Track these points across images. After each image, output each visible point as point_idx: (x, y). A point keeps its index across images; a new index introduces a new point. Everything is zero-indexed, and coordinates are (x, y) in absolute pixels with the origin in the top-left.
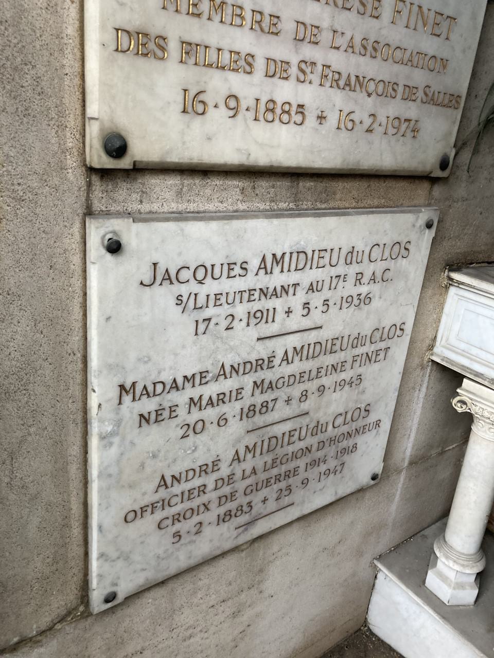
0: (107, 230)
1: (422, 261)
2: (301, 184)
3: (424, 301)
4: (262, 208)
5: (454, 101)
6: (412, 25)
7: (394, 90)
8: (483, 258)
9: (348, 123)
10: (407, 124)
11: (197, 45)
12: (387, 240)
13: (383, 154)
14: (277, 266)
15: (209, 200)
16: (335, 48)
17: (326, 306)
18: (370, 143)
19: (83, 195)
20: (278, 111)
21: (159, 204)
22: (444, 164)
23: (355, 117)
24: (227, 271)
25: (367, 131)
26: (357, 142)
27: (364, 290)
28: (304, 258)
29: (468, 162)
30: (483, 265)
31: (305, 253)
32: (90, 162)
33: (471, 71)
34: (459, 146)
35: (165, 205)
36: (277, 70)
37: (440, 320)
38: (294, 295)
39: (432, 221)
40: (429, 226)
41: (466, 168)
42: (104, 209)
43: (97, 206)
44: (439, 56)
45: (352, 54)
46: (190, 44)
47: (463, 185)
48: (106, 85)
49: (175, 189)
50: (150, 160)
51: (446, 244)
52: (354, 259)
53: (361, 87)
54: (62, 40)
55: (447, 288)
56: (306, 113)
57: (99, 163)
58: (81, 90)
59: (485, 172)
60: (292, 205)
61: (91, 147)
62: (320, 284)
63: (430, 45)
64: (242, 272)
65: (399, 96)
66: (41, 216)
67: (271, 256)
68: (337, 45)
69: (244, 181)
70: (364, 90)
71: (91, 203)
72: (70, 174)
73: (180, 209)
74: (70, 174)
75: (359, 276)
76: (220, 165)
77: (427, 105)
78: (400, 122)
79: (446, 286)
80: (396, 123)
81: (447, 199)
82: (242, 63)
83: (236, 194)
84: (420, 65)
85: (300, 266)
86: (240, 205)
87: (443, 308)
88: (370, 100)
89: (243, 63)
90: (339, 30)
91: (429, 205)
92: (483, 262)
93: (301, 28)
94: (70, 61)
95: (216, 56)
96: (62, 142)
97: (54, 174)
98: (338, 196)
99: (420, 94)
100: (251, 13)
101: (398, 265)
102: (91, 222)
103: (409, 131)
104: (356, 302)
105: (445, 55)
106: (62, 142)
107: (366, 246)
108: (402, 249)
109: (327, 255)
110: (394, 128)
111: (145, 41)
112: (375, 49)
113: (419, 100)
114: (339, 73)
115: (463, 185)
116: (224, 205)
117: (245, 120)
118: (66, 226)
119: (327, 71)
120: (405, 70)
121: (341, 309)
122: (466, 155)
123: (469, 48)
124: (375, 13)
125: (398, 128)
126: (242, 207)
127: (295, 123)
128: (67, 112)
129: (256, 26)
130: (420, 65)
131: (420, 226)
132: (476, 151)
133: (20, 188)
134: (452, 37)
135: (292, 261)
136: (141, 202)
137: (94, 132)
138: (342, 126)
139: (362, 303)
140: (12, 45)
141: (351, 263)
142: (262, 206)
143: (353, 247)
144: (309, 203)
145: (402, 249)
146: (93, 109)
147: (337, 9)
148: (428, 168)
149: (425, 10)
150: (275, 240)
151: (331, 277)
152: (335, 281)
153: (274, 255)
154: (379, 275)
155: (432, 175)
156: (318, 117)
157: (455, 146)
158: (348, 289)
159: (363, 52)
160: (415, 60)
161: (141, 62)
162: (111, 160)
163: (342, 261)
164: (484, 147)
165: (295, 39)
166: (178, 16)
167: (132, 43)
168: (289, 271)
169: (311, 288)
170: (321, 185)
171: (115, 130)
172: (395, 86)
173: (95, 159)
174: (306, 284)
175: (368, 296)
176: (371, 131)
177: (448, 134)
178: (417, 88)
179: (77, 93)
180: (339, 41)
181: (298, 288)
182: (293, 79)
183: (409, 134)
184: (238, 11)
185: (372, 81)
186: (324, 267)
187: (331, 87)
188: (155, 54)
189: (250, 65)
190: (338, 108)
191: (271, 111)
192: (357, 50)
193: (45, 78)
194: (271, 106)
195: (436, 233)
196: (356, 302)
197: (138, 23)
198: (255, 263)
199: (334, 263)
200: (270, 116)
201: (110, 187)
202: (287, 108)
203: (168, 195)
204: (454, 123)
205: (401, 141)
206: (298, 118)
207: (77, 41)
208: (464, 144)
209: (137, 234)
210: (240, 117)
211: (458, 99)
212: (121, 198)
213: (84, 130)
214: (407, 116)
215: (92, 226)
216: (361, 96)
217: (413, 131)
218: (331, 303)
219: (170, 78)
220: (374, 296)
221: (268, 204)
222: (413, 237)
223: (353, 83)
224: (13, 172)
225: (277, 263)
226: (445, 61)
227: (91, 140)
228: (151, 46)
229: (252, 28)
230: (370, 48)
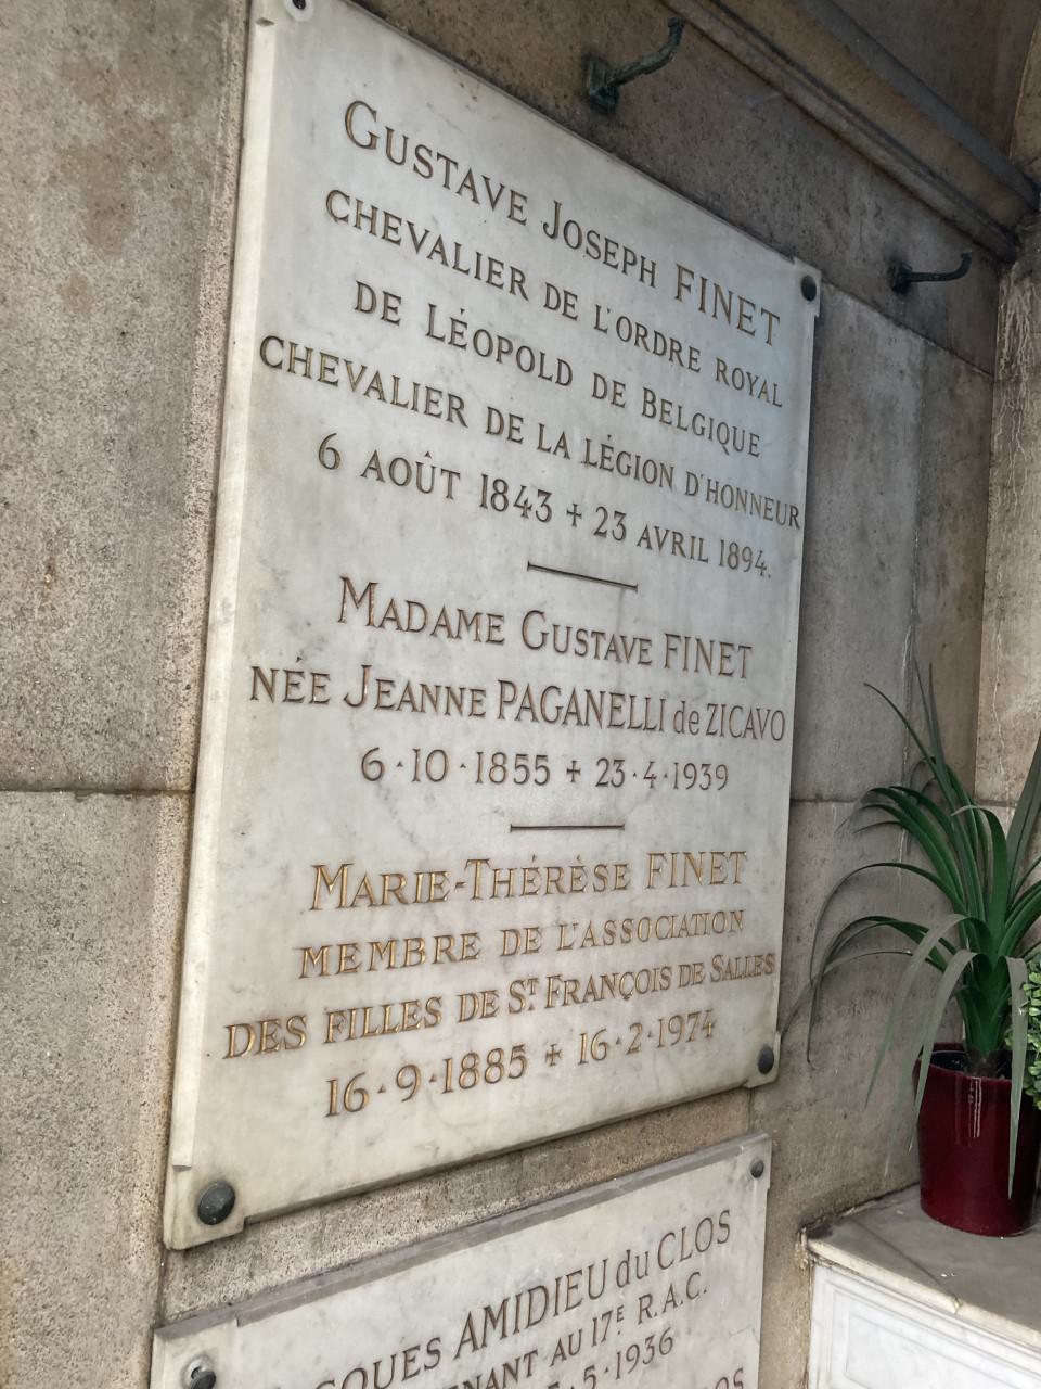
0: (192, 1355)
1: (756, 1239)
2: (526, 1161)
3: (772, 1307)
4: (460, 1222)
5: (764, 964)
6: (679, 880)
7: (664, 977)
8: (865, 1194)
9: (597, 1050)
10: (693, 1020)
11: (351, 1011)
12: (686, 1219)
13: (661, 1077)
14: (494, 1327)
15: (369, 1234)
16: (565, 948)
17: (522, 770)
18: (636, 1069)
19: (152, 1292)
20: (482, 1066)
21: (281, 1271)
22: (765, 1063)
23: (609, 1037)
24: (402, 1366)
25: (629, 1052)
26: (615, 1073)
27: (656, 1326)
28: (542, 1297)
29: (806, 1039)
30: (868, 1205)
31: (543, 1288)
32: (172, 1243)
33: (781, 905)
34: (783, 1028)
35: (292, 1267)
36: (479, 1006)
37: (808, 1336)
38: (529, 1374)
39: (761, 1164)
40: (757, 1173)
41: (804, 1050)
42: (186, 1307)
43: (175, 1305)
44: (727, 908)
45: (592, 949)
46: (341, 1013)
47: (806, 1077)
48: (205, 1111)
49: (310, 1234)
50: (273, 1207)
51: (795, 1189)
52: (633, 1272)
53: (612, 990)
54: (143, 1057)
55: (810, 1269)
56: (527, 1056)
57: (186, 1240)
58: (164, 1121)
59: (838, 1047)
60: (513, 1202)
61: (175, 1217)
62: (575, 1339)
63: (710, 899)
64: (430, 1360)
65: (675, 982)
66: (76, 1352)
67: (483, 1312)
68: (567, 944)
69: (429, 1185)
70: (617, 992)
71: (165, 1304)
72: (134, 1264)
73: (318, 1267)
74: (134, 1264)
75: (646, 1302)
76: (392, 1179)
77: (721, 983)
78: (682, 1022)
79: (808, 1267)
80: (676, 1025)
81: (780, 1111)
82: (423, 1013)
83: (415, 1210)
84: (700, 931)
85: (536, 1316)
86: (423, 1228)
87: (810, 1311)
88: (628, 1005)
89: (424, 1014)
90: (569, 920)
91: (752, 1131)
92: (866, 1201)
93: (512, 937)
94: (153, 1085)
95: (381, 1017)
96: (125, 1214)
97: (106, 1271)
98: (592, 1162)
99: (708, 971)
100: (406, 607)
101: (713, 1258)
102: (164, 1348)
103: (698, 1030)
104: (645, 1353)
105: (736, 906)
106: (125, 1214)
107: (651, 1242)
108: (716, 1226)
109: (583, 1281)
110: (673, 1033)
111: (272, 1029)
112: (627, 931)
113: (707, 979)
114: (559, 869)
115: (806, 1077)
116: (395, 1235)
117: (429, 1097)
118: (117, 1359)
119: (556, 984)
120: (680, 943)
121: (618, 1377)
122: (800, 1031)
123: (773, 883)
124: (621, 883)
125: (680, 1032)
126: (424, 1230)
127: (511, 1076)
128: (139, 1162)
129: (442, 957)
130: (700, 931)
131: (742, 1177)
132: (815, 1020)
133: (46, 1313)
134: (743, 878)
135: (521, 1314)
136: (251, 1275)
137: (181, 1192)
138: (588, 1057)
139: (657, 1353)
140: (64, 1087)
141: (627, 1282)
142: (461, 1218)
143: (628, 1251)
144: (543, 1189)
145: (716, 1226)
146: (181, 1153)
147: (563, 896)
148: (739, 1077)
149: (696, 856)
150: (489, 1281)
151: (595, 1320)
152: (601, 1325)
153: (488, 1309)
154: (680, 1289)
155: (749, 1086)
156: (548, 1055)
157: (778, 1029)
158: (630, 1332)
159: (609, 940)
160: (692, 926)
161: (266, 1061)
162: (208, 1228)
163: (611, 1282)
164: (828, 1009)
165: (503, 955)
166: (324, 981)
167: (253, 1037)
168: (517, 1330)
169: (560, 1353)
170: (559, 1154)
171: (217, 1177)
172: (666, 972)
173: (181, 1233)
174: (548, 1347)
175: (666, 1336)
176: (636, 1050)
177: (765, 1013)
178: (701, 964)
179: (158, 1127)
180: (570, 937)
181: (535, 1358)
182: (503, 1013)
183: (700, 1035)
184: (414, 945)
185: (629, 976)
186: (579, 1304)
187: (565, 1004)
188: (286, 1043)
189: (435, 1013)
190: (578, 1031)
191: (471, 1071)
192: (599, 941)
193: (109, 1121)
194: (470, 1062)
195: (772, 1184)
196: (645, 1353)
197: (262, 1009)
198: (453, 1334)
199: (596, 1291)
200: (469, 1079)
201: (200, 1265)
202: (495, 1057)
203: (298, 1249)
204: (771, 994)
205: (688, 1050)
206: (516, 1067)
207: (165, 1051)
208: (795, 1013)
209: (243, 1348)
210: (420, 1095)
211: (771, 959)
212: (216, 1280)
213: (164, 1183)
214: (692, 1009)
215: (167, 1356)
216: (615, 1003)
217: (705, 1028)
218: (598, 1372)
219: (309, 1071)
220: (677, 1334)
221: (471, 1211)
222: (732, 1200)
223: (598, 988)
224: (38, 1289)
225: (494, 1323)
226: (738, 914)
227: (176, 1206)
228: (282, 1033)
229: (436, 961)
230: (619, 931)
